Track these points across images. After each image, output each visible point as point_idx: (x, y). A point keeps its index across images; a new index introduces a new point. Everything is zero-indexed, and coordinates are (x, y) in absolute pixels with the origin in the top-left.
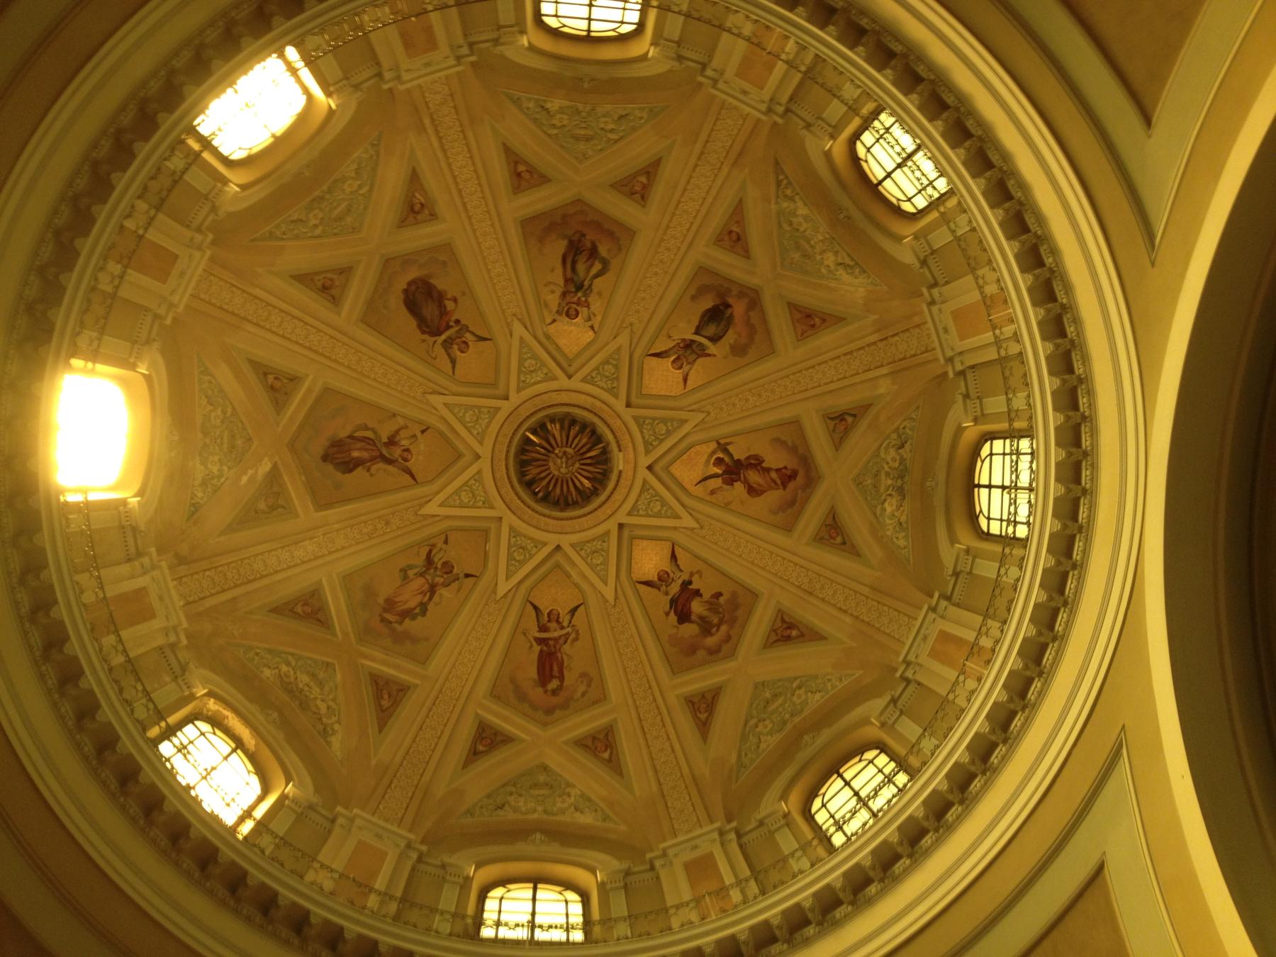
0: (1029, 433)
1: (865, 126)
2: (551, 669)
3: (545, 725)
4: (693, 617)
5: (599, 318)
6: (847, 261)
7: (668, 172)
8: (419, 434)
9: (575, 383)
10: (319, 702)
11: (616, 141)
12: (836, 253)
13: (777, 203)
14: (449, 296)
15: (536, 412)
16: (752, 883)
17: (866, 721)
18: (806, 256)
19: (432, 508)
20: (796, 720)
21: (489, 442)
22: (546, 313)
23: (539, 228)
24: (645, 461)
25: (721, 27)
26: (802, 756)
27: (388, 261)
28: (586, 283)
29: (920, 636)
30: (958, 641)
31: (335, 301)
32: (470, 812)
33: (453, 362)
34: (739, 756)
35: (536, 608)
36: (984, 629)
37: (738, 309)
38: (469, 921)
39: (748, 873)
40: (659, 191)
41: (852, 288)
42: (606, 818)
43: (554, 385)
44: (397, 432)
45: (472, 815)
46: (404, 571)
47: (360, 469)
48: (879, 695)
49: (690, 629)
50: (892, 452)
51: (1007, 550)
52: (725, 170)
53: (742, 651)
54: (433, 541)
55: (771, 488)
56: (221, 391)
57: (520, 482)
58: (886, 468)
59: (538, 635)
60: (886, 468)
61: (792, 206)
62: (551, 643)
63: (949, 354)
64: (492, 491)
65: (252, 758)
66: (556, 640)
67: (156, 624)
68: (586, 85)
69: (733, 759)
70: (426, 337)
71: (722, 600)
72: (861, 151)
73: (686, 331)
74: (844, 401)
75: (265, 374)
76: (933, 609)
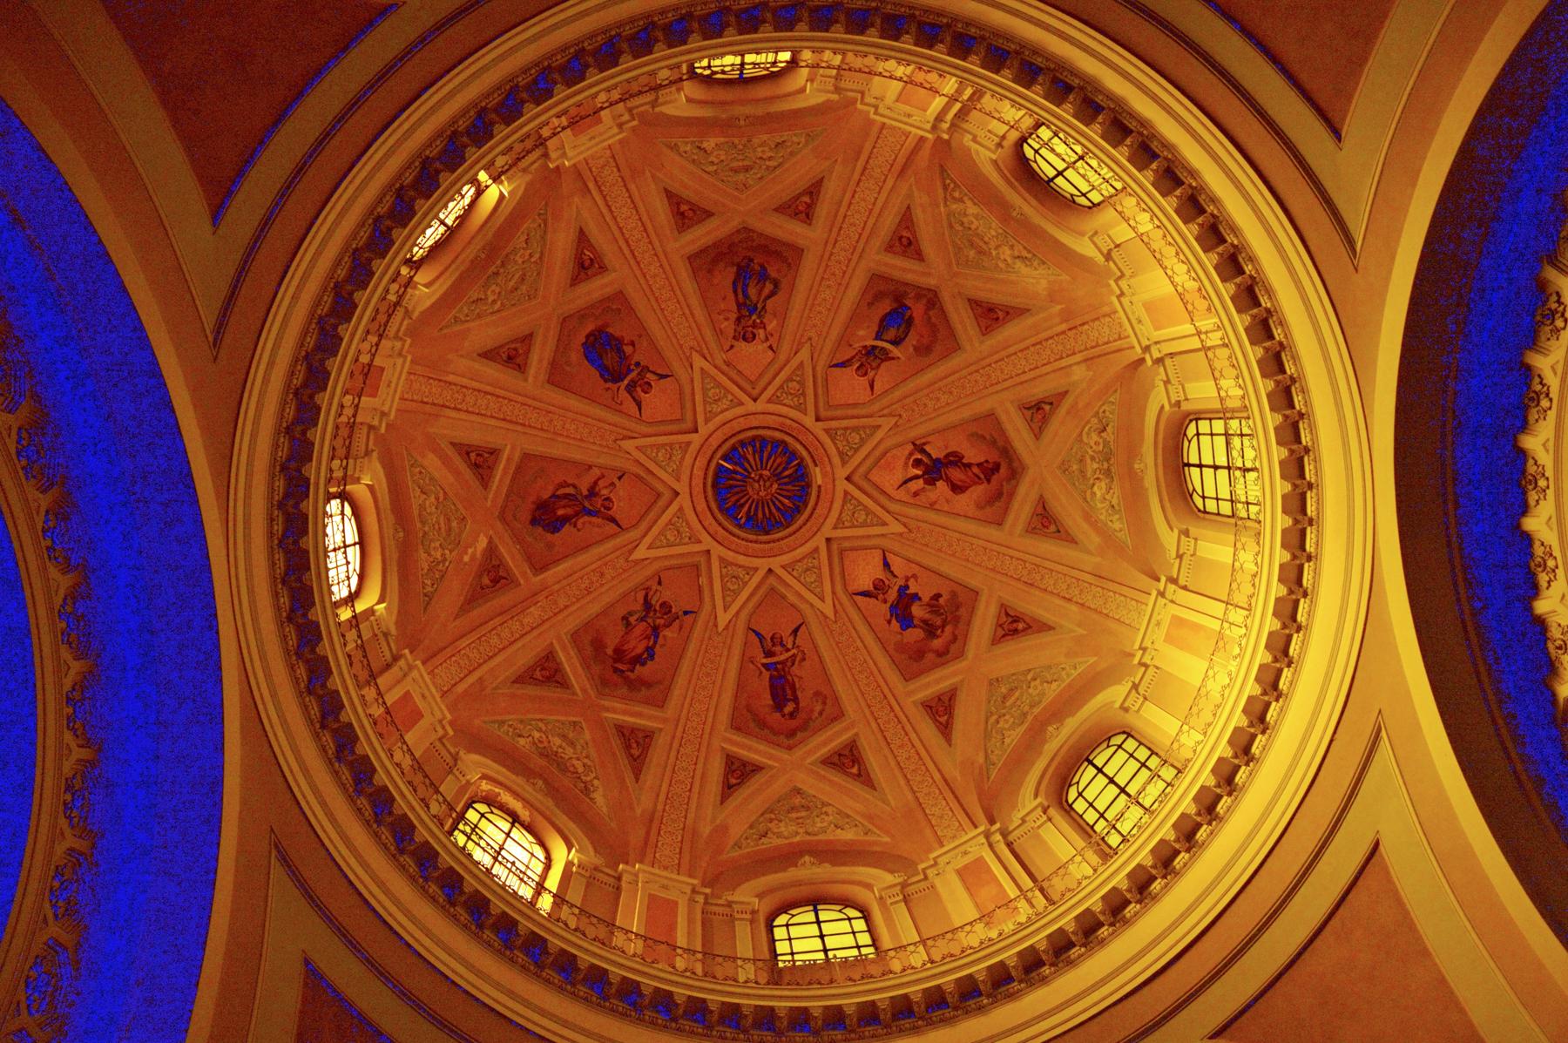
3: (790, 748)
4: (916, 622)
5: (776, 336)
6: (1025, 254)
7: (831, 189)
9: (760, 406)
10: (575, 762)
12: (1012, 247)
13: (946, 205)
18: (980, 252)
19: (723, 619)
20: (1036, 711)
23: (705, 261)
24: (842, 473)
31: (521, 368)
32: (738, 845)
34: (987, 756)
35: (757, 634)
37: (917, 310)
40: (822, 211)
44: (596, 483)
46: (625, 618)
48: (1119, 681)
50: (1095, 437)
52: (890, 183)
53: (971, 651)
55: (975, 483)
56: (431, 479)
57: (720, 509)
63: (1145, 343)
65: (529, 828)
66: (783, 663)
69: (981, 759)
70: (609, 385)
71: (941, 601)
72: (1029, 153)
73: (865, 336)
76: (1162, 594)
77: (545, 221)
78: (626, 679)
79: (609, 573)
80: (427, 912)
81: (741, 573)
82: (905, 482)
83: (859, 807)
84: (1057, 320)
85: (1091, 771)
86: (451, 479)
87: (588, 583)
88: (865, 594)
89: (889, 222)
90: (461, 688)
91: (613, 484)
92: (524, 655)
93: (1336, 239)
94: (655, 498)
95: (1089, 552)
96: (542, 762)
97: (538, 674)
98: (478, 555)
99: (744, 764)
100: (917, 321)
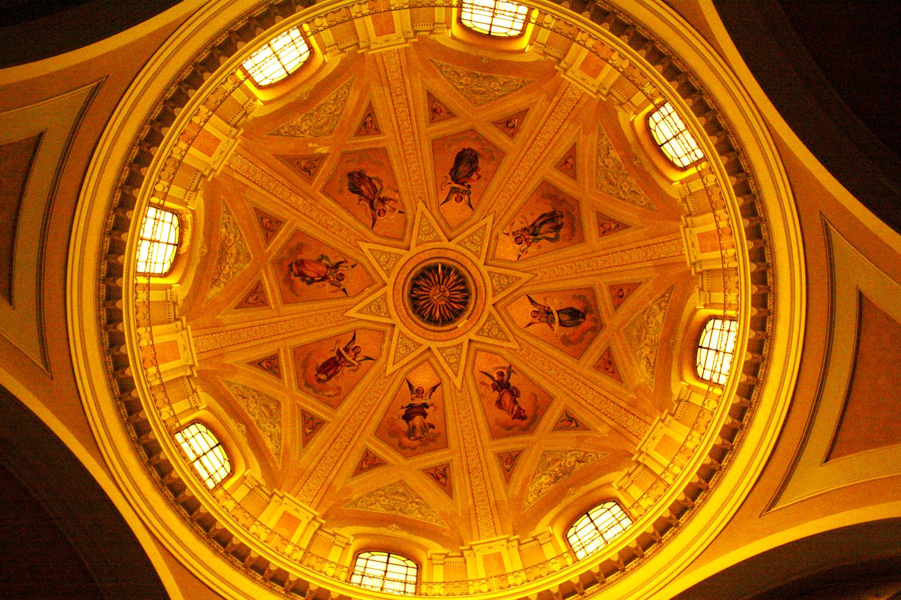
0: (634, 520)
1: (723, 318)
2: (329, 370)
3: (300, 388)
4: (411, 423)
6: (652, 361)
8: (397, 211)
9: (484, 269)
10: (227, 267)
11: (620, 198)
12: (651, 352)
14: (479, 173)
15: (454, 261)
16: (302, 553)
17: (426, 549)
20: (400, 514)
21: (421, 248)
22: (508, 228)
23: (547, 191)
24: (472, 335)
25: (713, 210)
26: (382, 530)
27: (473, 130)
28: (539, 236)
29: (490, 545)
30: (502, 565)
31: (432, 120)
33: (447, 200)
35: (354, 337)
36: (516, 574)
37: (587, 323)
38: (177, 425)
39: (304, 547)
40: (613, 238)
41: (640, 375)
42: (277, 454)
43: (475, 259)
44: (391, 199)
45: (229, 386)
46: (323, 257)
47: (357, 195)
49: (404, 426)
50: (573, 459)
51: (566, 555)
52: (650, 264)
54: (349, 260)
56: (345, 101)
57: (413, 279)
58: (563, 462)
59: (341, 349)
60: (563, 462)
61: (658, 311)
62: (343, 359)
63: (644, 449)
64: (396, 270)
65: (177, 256)
66: (346, 360)
67: (209, 160)
68: (635, 163)
69: (355, 497)
71: (431, 430)
73: (554, 305)
74: (579, 414)
75: (369, 115)
76: (508, 541)
77: (521, 87)
78: (289, 274)
79: (344, 233)
80: (102, 200)
81: (384, 310)
82: (486, 374)
83: (289, 442)
84: (626, 400)
85: (385, 559)
86: (350, 113)
87: (334, 225)
88: (410, 385)
89: (625, 278)
90: (236, 176)
91: (394, 209)
92: (272, 208)
93: (771, 494)
94: (399, 238)
95: (506, 491)
96: (218, 248)
97: (265, 221)
98: (316, 151)
99: (278, 367)
100: (580, 328)
